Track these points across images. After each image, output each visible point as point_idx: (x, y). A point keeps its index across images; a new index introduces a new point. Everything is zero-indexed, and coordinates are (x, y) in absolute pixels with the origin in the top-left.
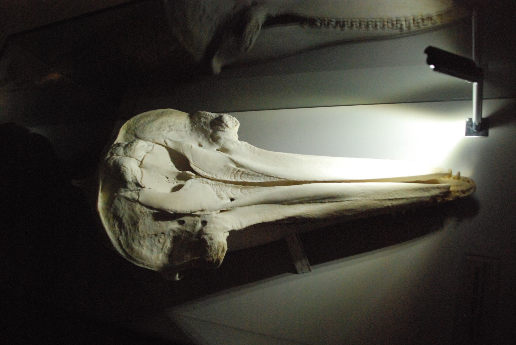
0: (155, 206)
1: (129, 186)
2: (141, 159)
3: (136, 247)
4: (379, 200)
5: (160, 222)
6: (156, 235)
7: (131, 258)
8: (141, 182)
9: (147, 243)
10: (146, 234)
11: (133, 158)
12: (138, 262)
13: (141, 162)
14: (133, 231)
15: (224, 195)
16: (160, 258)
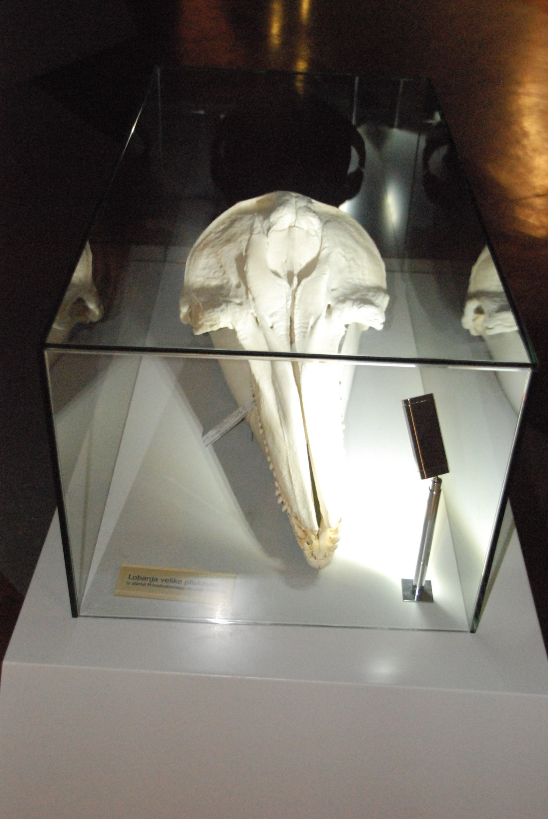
0: (249, 252)
1: (266, 221)
2: (297, 224)
3: (206, 252)
4: (287, 461)
5: (235, 265)
6: (221, 267)
7: (195, 251)
8: (272, 231)
9: (212, 261)
10: (220, 256)
11: (296, 216)
12: (191, 258)
13: (294, 226)
14: (221, 242)
15: (275, 319)
16: (199, 279)
